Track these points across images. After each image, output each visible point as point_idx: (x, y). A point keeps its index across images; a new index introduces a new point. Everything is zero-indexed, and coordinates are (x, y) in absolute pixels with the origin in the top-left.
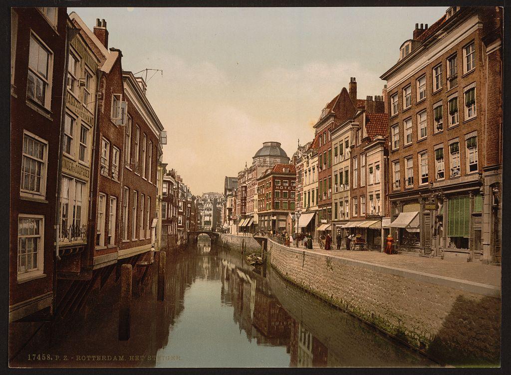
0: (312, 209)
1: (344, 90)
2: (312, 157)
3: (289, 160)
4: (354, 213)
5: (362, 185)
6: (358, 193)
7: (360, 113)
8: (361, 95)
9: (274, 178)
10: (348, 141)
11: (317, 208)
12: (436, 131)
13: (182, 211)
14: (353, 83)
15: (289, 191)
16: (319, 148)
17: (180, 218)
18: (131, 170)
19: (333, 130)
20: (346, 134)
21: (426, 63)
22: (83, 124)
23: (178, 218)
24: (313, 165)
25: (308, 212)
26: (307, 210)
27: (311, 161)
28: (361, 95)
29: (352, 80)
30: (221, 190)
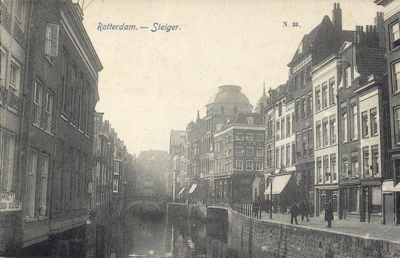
0: (288, 169)
1: (326, 17)
3: (253, 108)
4: (355, 213)
7: (349, 47)
8: (348, 25)
11: (294, 168)
13: (118, 174)
14: (337, 11)
15: (255, 147)
16: (296, 89)
17: (115, 183)
18: (66, 120)
19: (317, 60)
20: (325, 75)
21: (392, 12)
22: (14, 61)
23: (112, 183)
25: (283, 173)
26: (280, 173)
27: (284, 108)
28: (348, 25)
29: (335, 7)
30: (167, 149)
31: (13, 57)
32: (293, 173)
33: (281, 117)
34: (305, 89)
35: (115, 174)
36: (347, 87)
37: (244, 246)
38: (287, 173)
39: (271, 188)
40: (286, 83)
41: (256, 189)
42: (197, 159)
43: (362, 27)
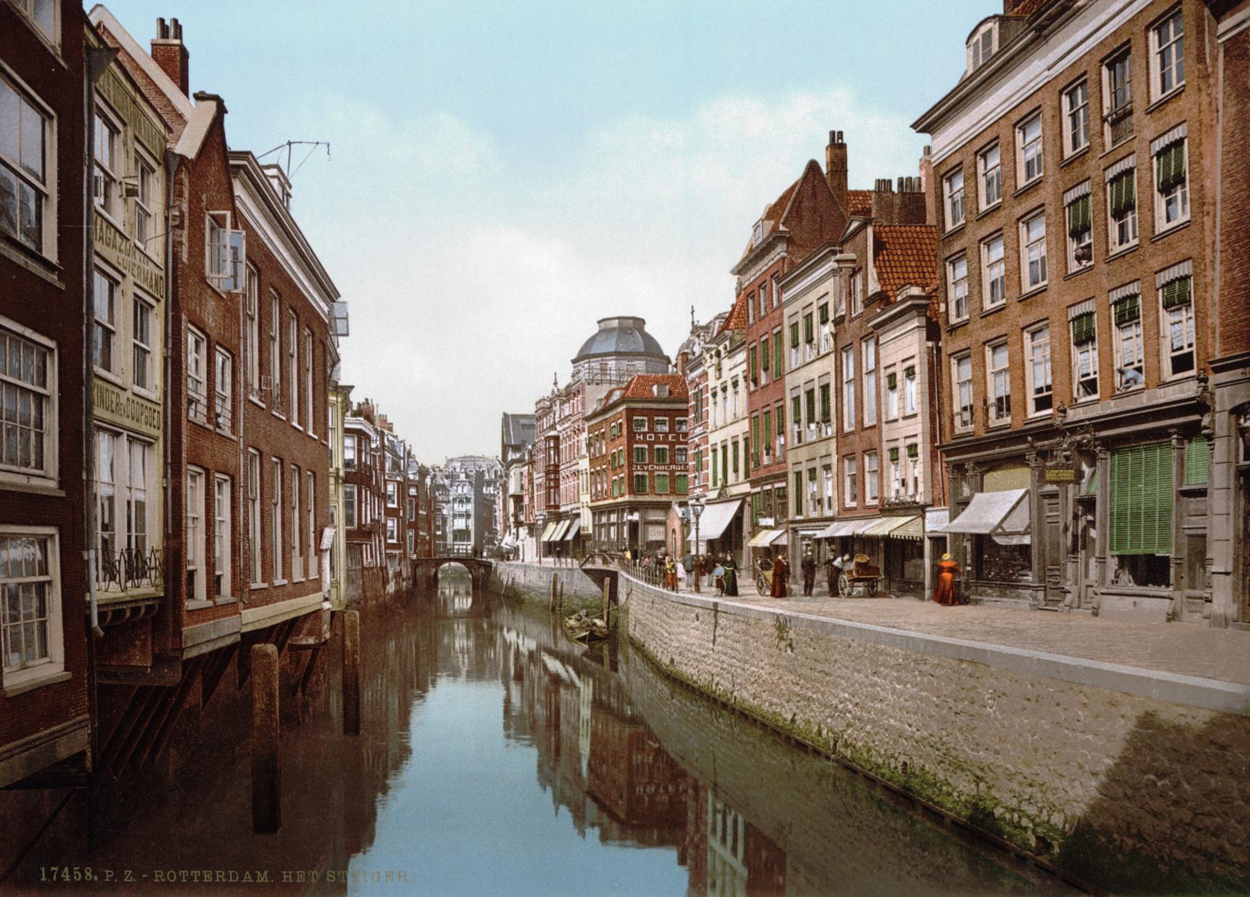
2: (729, 352)
5: (867, 423)
6: (858, 445)
9: (630, 413)
10: (797, 323)
12: (1074, 266)
13: (395, 506)
14: (837, 146)
15: (672, 444)
16: (747, 328)
17: (390, 523)
20: (820, 287)
24: (734, 372)
25: (723, 498)
26: (720, 495)
27: (726, 363)
29: (832, 139)
31: (292, 308)
32: (743, 497)
33: (722, 380)
34: (766, 323)
35: (390, 505)
36: (854, 315)
37: (718, 761)
38: (732, 499)
39: (697, 529)
40: (730, 309)
41: (916, 479)
42: (735, 567)
43: (890, 181)
